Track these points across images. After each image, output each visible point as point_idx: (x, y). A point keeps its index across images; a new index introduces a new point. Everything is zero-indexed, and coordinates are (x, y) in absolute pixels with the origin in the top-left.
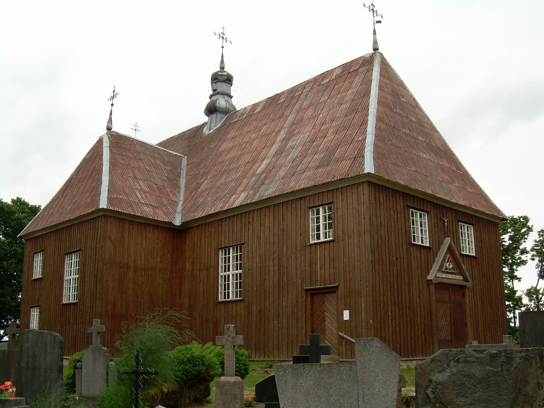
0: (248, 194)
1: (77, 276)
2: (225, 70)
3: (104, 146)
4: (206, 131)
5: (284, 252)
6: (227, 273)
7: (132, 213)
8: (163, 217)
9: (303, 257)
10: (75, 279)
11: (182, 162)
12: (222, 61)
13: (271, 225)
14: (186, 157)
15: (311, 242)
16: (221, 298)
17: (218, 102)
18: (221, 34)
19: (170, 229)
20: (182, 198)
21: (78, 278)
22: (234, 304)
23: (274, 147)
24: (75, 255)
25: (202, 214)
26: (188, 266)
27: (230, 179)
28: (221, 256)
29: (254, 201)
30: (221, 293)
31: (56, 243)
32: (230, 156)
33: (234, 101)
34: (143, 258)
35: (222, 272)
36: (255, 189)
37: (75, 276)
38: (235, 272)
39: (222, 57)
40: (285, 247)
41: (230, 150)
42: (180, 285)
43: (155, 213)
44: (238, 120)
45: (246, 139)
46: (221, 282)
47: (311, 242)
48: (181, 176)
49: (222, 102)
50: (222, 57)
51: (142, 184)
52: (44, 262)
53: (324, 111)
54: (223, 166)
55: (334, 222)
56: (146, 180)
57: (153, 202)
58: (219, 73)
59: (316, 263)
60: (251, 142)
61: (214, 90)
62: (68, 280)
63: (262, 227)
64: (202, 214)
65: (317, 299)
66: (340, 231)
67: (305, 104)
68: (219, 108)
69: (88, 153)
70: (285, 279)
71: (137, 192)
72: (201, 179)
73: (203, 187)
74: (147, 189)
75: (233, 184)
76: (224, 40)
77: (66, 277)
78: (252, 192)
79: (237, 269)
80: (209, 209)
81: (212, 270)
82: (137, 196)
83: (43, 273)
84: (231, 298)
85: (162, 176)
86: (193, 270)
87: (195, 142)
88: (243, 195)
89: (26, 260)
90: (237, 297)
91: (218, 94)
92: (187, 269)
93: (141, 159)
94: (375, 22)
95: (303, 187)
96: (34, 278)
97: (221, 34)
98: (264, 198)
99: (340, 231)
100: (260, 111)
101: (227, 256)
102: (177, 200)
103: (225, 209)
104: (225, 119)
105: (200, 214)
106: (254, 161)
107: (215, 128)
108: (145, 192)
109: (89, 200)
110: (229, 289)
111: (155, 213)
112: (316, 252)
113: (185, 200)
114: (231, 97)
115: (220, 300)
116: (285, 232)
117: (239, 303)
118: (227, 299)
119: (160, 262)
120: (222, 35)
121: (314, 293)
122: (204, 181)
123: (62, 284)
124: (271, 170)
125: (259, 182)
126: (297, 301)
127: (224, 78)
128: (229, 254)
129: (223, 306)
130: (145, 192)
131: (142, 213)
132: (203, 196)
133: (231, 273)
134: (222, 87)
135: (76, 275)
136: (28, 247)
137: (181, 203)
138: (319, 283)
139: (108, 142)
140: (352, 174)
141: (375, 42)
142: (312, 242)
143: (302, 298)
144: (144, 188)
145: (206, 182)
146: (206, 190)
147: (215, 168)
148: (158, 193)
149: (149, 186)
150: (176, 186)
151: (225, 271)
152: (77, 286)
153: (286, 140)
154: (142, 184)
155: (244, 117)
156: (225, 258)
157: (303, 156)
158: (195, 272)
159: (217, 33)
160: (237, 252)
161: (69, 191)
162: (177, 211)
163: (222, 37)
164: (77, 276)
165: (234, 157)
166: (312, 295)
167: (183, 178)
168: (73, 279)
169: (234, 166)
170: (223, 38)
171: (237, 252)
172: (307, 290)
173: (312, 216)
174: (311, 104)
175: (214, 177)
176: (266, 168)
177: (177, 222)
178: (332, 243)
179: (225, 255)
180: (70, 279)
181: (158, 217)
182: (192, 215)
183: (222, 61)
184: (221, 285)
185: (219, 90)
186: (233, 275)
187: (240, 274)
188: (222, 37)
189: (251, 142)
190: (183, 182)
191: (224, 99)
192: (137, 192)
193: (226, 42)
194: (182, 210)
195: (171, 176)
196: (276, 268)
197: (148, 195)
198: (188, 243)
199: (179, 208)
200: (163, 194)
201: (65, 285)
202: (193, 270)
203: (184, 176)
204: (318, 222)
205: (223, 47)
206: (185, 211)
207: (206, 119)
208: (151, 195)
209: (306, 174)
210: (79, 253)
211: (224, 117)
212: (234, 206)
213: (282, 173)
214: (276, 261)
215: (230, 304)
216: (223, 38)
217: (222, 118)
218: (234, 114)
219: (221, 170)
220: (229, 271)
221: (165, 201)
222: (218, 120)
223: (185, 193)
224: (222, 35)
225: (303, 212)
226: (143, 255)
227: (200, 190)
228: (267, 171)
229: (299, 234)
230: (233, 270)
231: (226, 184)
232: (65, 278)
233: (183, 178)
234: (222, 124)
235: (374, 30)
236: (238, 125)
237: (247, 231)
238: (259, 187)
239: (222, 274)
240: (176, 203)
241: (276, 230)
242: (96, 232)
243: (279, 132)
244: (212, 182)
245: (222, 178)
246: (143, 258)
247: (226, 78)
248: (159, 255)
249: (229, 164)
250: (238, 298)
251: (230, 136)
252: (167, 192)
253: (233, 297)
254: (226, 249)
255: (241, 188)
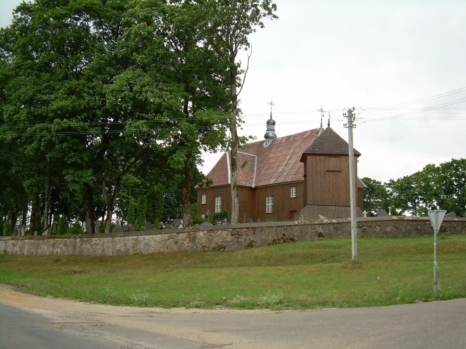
1: (221, 204)
2: (272, 119)
4: (265, 146)
6: (269, 204)
12: (271, 115)
19: (250, 188)
20: (255, 176)
26: (257, 201)
27: (271, 172)
28: (267, 199)
33: (276, 132)
36: (277, 178)
38: (271, 204)
39: (271, 113)
43: (246, 183)
44: (276, 144)
45: (278, 155)
49: (271, 134)
50: (271, 113)
51: (241, 172)
52: (206, 198)
60: (279, 157)
61: (268, 128)
65: (292, 213)
69: (221, 158)
71: (240, 176)
72: (262, 169)
73: (262, 173)
74: (243, 174)
75: (271, 174)
82: (240, 178)
83: (206, 202)
84: (269, 212)
89: (198, 197)
91: (269, 130)
95: (289, 181)
105: (260, 184)
106: (279, 166)
108: (242, 175)
111: (246, 183)
113: (256, 177)
117: (272, 214)
120: (271, 103)
121: (291, 212)
125: (279, 176)
130: (242, 175)
131: (242, 184)
133: (270, 204)
134: (271, 127)
136: (199, 193)
137: (254, 178)
140: (301, 180)
141: (321, 124)
142: (291, 197)
144: (242, 174)
146: (263, 174)
148: (246, 175)
149: (244, 173)
150: (253, 171)
154: (241, 172)
159: (269, 103)
164: (221, 204)
170: (271, 104)
172: (289, 211)
175: (266, 169)
177: (253, 186)
183: (271, 115)
189: (279, 157)
190: (255, 168)
194: (255, 181)
197: (243, 176)
199: (254, 180)
201: (216, 207)
204: (293, 191)
206: (256, 183)
208: (244, 176)
209: (291, 177)
216: (271, 104)
221: (249, 178)
223: (256, 174)
231: (269, 173)
236: (276, 146)
238: (278, 178)
240: (252, 178)
251: (273, 151)
255: (273, 177)
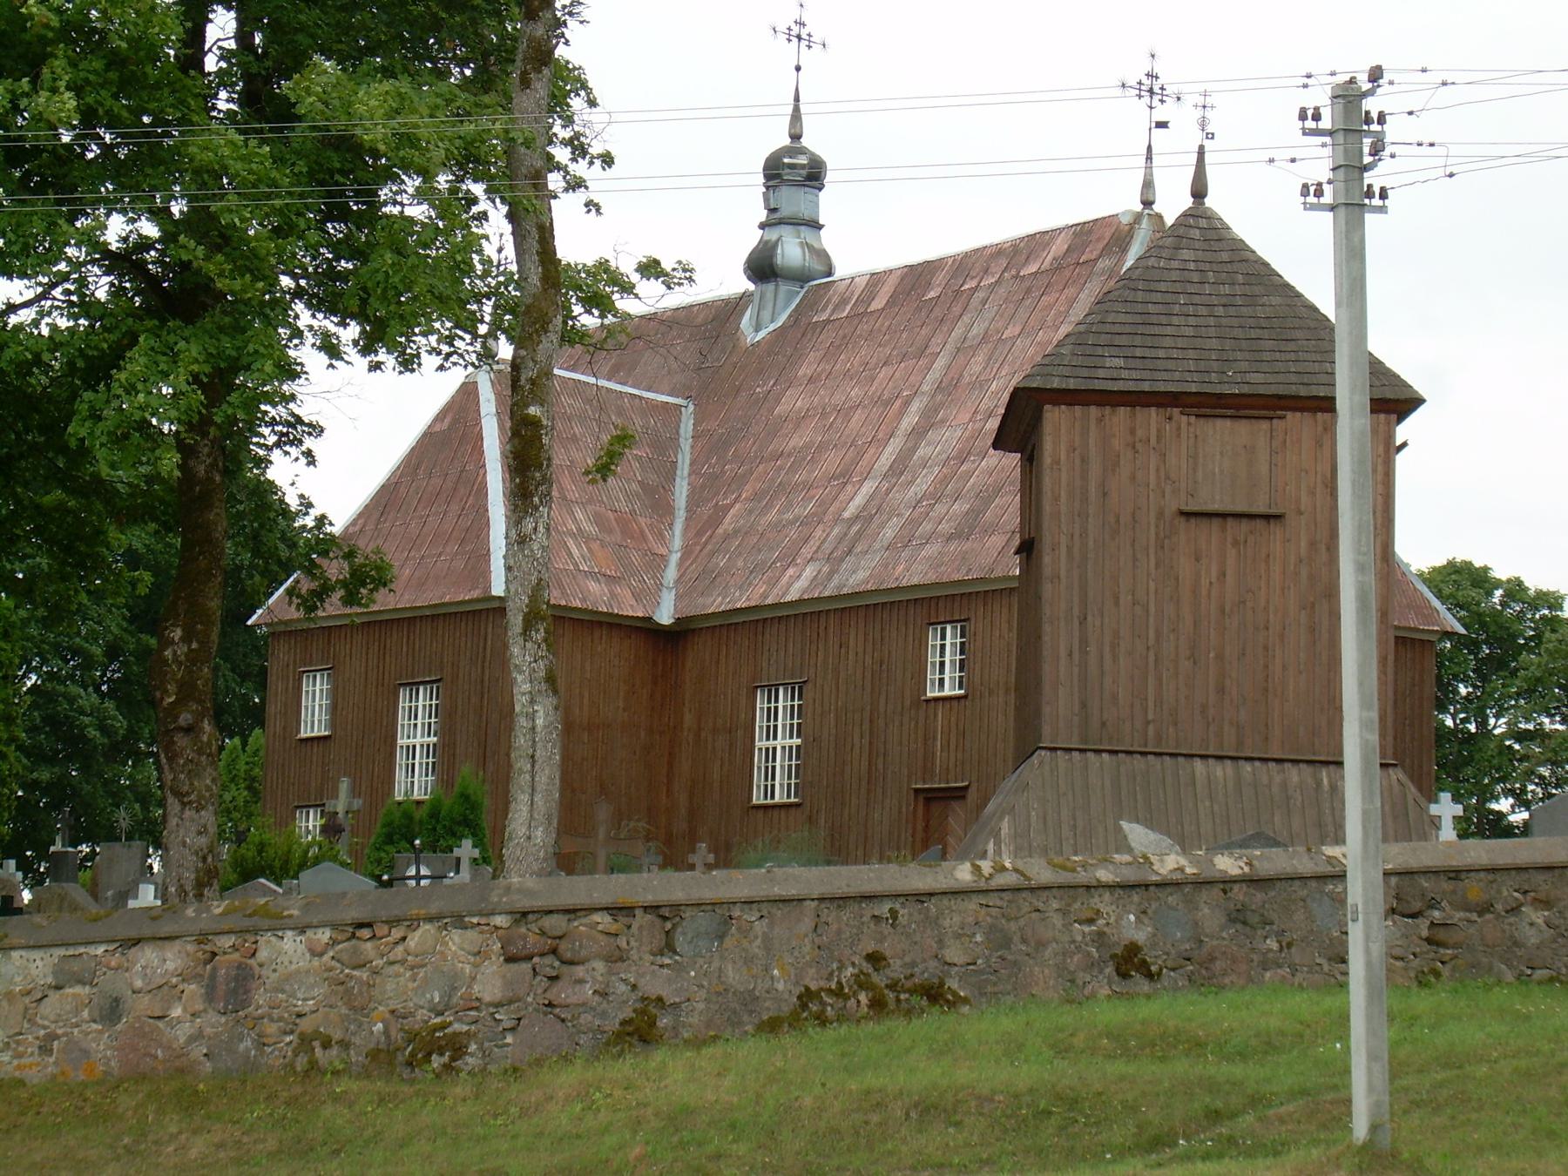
0: (819, 572)
3: (482, 414)
4: (751, 332)
5: (882, 710)
6: (771, 743)
7: (563, 603)
8: (632, 606)
9: (913, 724)
10: (428, 746)
11: (682, 425)
13: (860, 650)
14: (691, 408)
15: (929, 694)
16: (757, 798)
17: (779, 251)
18: (793, 26)
20: (677, 542)
21: (435, 745)
22: (783, 812)
23: (889, 449)
24: (425, 690)
25: (721, 604)
26: (688, 719)
27: (789, 516)
28: (761, 703)
29: (827, 594)
30: (759, 787)
31: (370, 656)
32: (796, 441)
33: (828, 239)
34: (586, 701)
35: (761, 740)
36: (834, 561)
37: (427, 739)
38: (788, 742)
40: (882, 701)
41: (800, 420)
42: (670, 765)
43: (613, 595)
44: (828, 321)
46: (760, 761)
47: (929, 694)
48: (678, 472)
49: (791, 252)
51: (580, 515)
53: (1003, 373)
54: (781, 468)
55: (968, 658)
56: (590, 501)
57: (609, 567)
58: (786, 160)
59: (935, 739)
60: (845, 412)
62: (408, 747)
63: (843, 650)
64: (721, 604)
65: (936, 809)
66: (977, 680)
67: (975, 331)
68: (782, 269)
70: (880, 766)
71: (571, 543)
73: (728, 524)
75: (793, 533)
76: (804, 43)
77: (402, 738)
78: (826, 569)
79: (791, 737)
80: (737, 594)
81: (740, 733)
82: (570, 554)
83: (333, 723)
85: (628, 481)
86: (700, 729)
87: (718, 360)
88: (809, 572)
89: (275, 683)
90: (789, 796)
91: (781, 222)
92: (685, 726)
93: (574, 439)
94: (1153, 125)
95: (915, 581)
96: (303, 735)
97: (793, 26)
98: (845, 591)
99: (977, 680)
100: (883, 309)
101: (773, 705)
102: (663, 551)
103: (769, 601)
104: (797, 300)
106: (844, 477)
107: (772, 327)
108: (588, 539)
109: (460, 564)
110: (773, 778)
111: (613, 595)
112: (935, 715)
113: (687, 552)
114: (820, 227)
115: (755, 801)
116: (884, 667)
117: (793, 811)
118: (769, 801)
119: (624, 710)
120: (796, 30)
122: (732, 505)
123: (392, 755)
124: (872, 517)
125: (844, 547)
126: (900, 812)
127: (800, 175)
128: (777, 701)
129: (760, 813)
130: (588, 539)
131: (584, 600)
132: (728, 551)
133: (779, 743)
134: (792, 200)
135: (429, 735)
136: (279, 659)
137: (675, 558)
138: (937, 779)
139: (492, 397)
141: (1148, 185)
142: (929, 694)
143: (908, 805)
145: (737, 506)
146: (736, 532)
147: (761, 467)
149: (598, 520)
151: (768, 739)
152: (434, 763)
153: (918, 433)
154: (580, 515)
155: (845, 314)
156: (769, 709)
157: (935, 496)
158: (703, 735)
159: (782, 28)
160: (793, 700)
161: (396, 519)
162: (665, 583)
163: (798, 35)
165: (807, 446)
166: (928, 800)
167: (682, 478)
168: (422, 746)
169: (803, 478)
170: (799, 37)
171: (793, 700)
172: (917, 791)
173: (933, 641)
174: (985, 338)
175: (757, 496)
176: (864, 508)
178: (963, 701)
179: (769, 702)
180: (414, 747)
181: (620, 607)
182: (700, 600)
184: (759, 768)
185: (785, 211)
186: (783, 748)
187: (798, 747)
188: (798, 35)
189: (845, 412)
190: (681, 492)
191: (799, 237)
192: (571, 543)
193: (809, 47)
194: (677, 581)
195: (652, 479)
196: (866, 741)
197: (595, 546)
198: (689, 664)
199: (671, 574)
200: (632, 538)
201: (400, 759)
202: (700, 729)
203: (686, 472)
205: (798, 69)
206: (685, 588)
207: (743, 284)
210: (438, 688)
211: (798, 293)
212: (788, 598)
213: (889, 533)
214: (866, 726)
215: (776, 813)
216: (799, 37)
217: (793, 295)
218: (822, 292)
219: (773, 480)
220: (775, 738)
221: (635, 557)
222: (780, 303)
223: (686, 529)
224: (796, 30)
225: (917, 631)
226: (586, 695)
227: (720, 531)
228: (865, 517)
229: (908, 675)
230: (784, 738)
231: (779, 527)
232: (399, 741)
233: (682, 478)
234: (790, 316)
235: (1149, 148)
236: (827, 337)
237: (813, 654)
238: (842, 560)
239: (760, 743)
241: (868, 660)
242: (481, 645)
243: (907, 403)
244: (751, 512)
245: (773, 506)
246: (586, 701)
247: (804, 172)
248: (622, 694)
249: (793, 469)
250: (793, 800)
251: (805, 370)
252: (642, 532)
253: (781, 797)
254: (772, 690)
255: (807, 551)
